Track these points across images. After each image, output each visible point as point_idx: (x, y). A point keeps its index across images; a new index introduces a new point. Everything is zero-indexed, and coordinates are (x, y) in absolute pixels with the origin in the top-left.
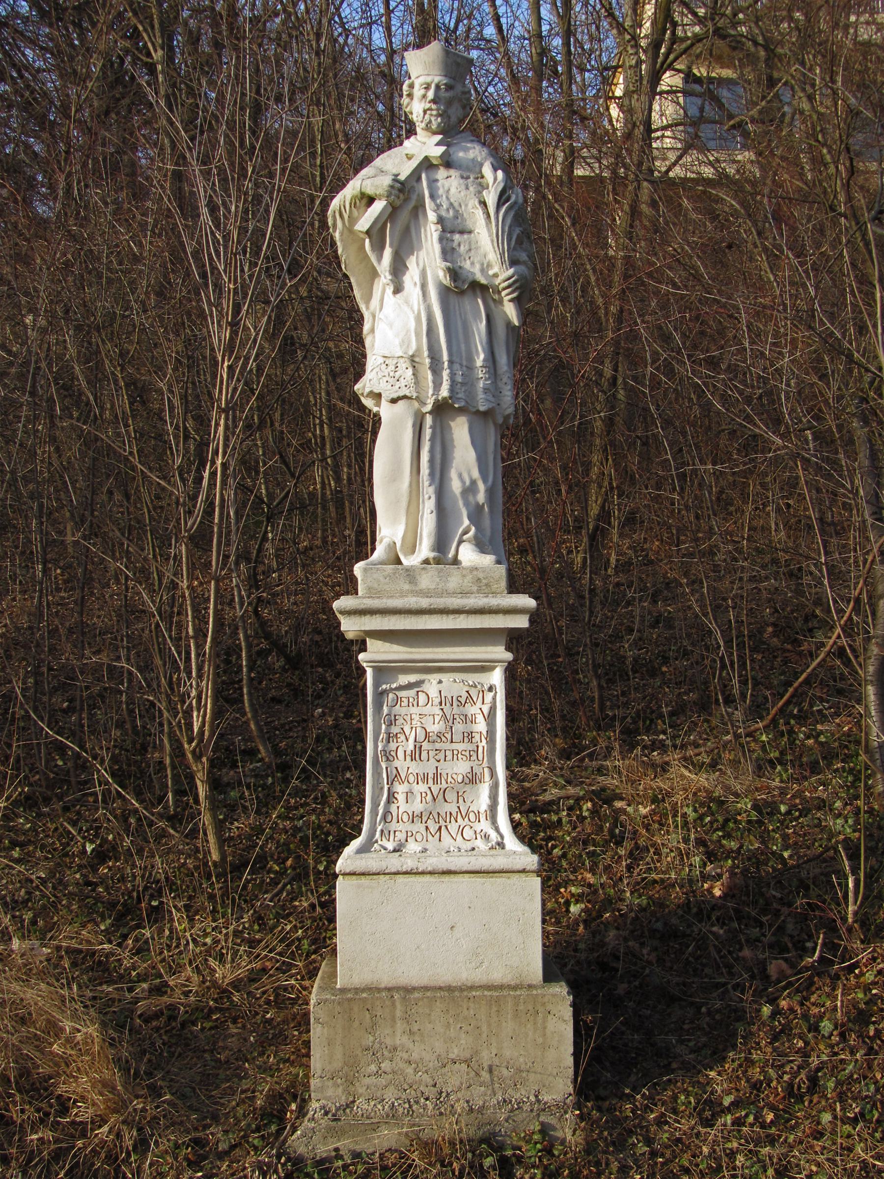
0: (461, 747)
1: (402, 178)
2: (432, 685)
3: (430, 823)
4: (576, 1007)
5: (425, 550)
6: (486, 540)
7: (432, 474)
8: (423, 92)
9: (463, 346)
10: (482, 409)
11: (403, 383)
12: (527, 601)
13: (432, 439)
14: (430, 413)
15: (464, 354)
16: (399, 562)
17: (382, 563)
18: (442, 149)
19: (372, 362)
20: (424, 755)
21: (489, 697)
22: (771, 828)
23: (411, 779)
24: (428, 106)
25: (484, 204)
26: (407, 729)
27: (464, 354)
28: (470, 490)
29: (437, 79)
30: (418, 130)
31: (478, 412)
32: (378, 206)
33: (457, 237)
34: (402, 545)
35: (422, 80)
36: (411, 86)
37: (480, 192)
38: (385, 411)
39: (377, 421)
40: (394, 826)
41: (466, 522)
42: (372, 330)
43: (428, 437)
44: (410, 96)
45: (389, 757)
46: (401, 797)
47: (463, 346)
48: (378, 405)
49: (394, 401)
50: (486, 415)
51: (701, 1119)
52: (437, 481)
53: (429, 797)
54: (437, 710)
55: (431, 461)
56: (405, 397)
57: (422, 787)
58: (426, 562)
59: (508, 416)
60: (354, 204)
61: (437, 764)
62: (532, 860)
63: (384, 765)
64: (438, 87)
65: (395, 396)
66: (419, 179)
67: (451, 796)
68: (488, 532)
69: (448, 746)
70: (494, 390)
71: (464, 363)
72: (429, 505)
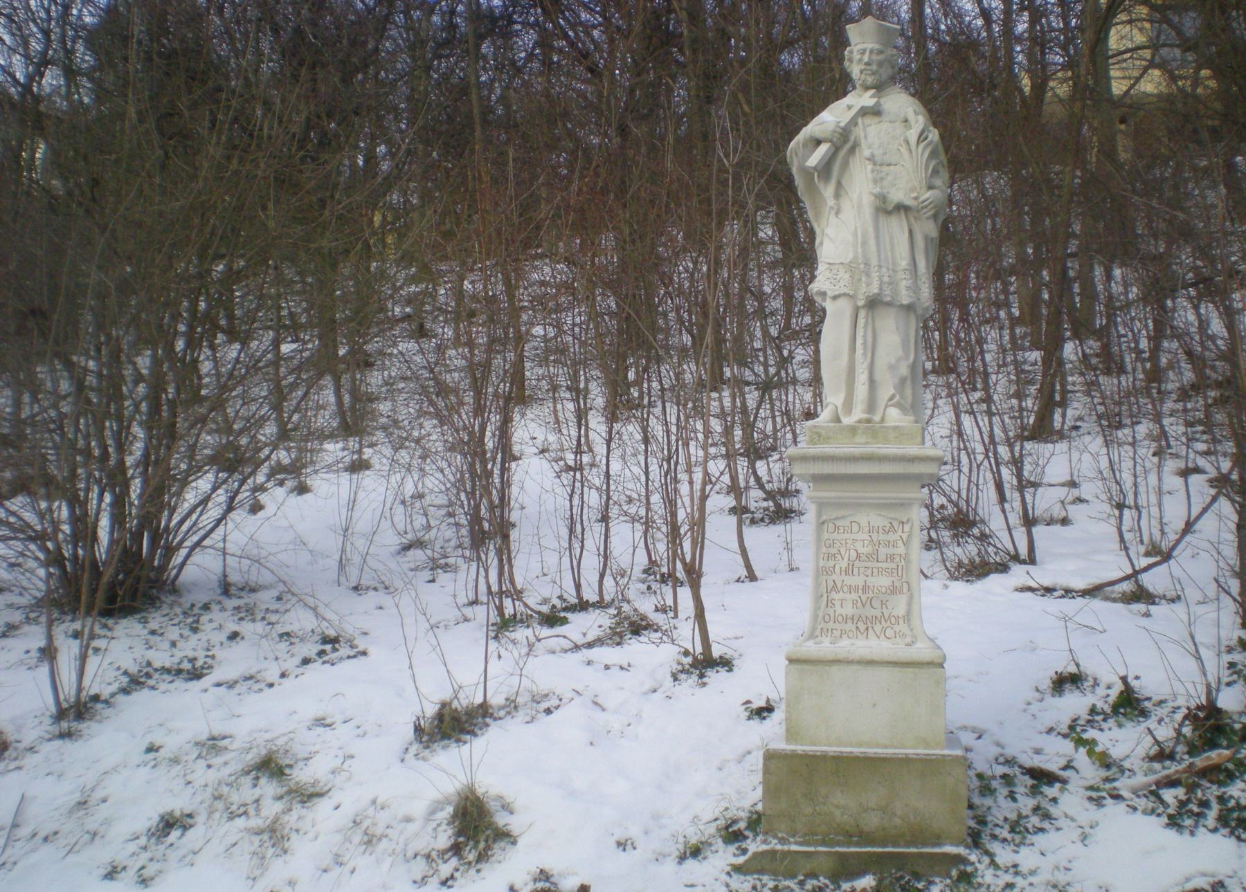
0: (884, 565)
1: (842, 124)
2: (863, 518)
3: (860, 625)
11: (842, 283)
14: (863, 307)
18: (875, 100)
19: (821, 269)
20: (856, 571)
23: (845, 589)
25: (907, 142)
26: (843, 552)
31: (902, 306)
32: (823, 148)
33: (885, 168)
36: (851, 52)
37: (1233, 376)
38: (829, 305)
39: (824, 311)
42: (821, 243)
44: (851, 60)
48: (824, 300)
49: (835, 298)
50: (909, 308)
51: (761, 303)
52: (869, 360)
53: (859, 604)
54: (866, 536)
55: (865, 344)
56: (844, 294)
59: (927, 308)
60: (805, 145)
64: (871, 52)
66: (856, 124)
67: (876, 603)
70: (915, 289)
72: (862, 378)
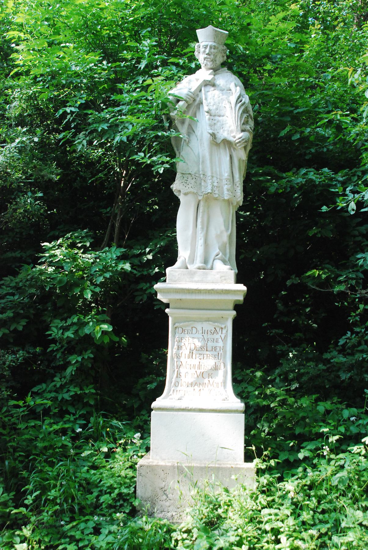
4: (246, 419)
5: (198, 263)
6: (227, 259)
7: (202, 228)
8: (204, 49)
9: (218, 169)
10: (226, 198)
12: (242, 287)
13: (204, 212)
15: (218, 173)
16: (187, 268)
17: (179, 268)
20: (194, 356)
21: (224, 331)
22: (68, 149)
23: (188, 367)
24: (206, 56)
27: (218, 173)
28: (219, 236)
29: (210, 43)
30: (202, 67)
34: (189, 260)
35: (204, 43)
40: (179, 388)
41: (218, 250)
43: (201, 211)
45: (178, 357)
46: (183, 374)
47: (218, 169)
52: (205, 229)
57: (193, 371)
58: (199, 268)
61: (200, 360)
62: (239, 405)
63: (175, 360)
65: (186, 191)
66: (201, 91)
68: (228, 255)
69: (205, 352)
71: (218, 177)
72: (200, 242)
